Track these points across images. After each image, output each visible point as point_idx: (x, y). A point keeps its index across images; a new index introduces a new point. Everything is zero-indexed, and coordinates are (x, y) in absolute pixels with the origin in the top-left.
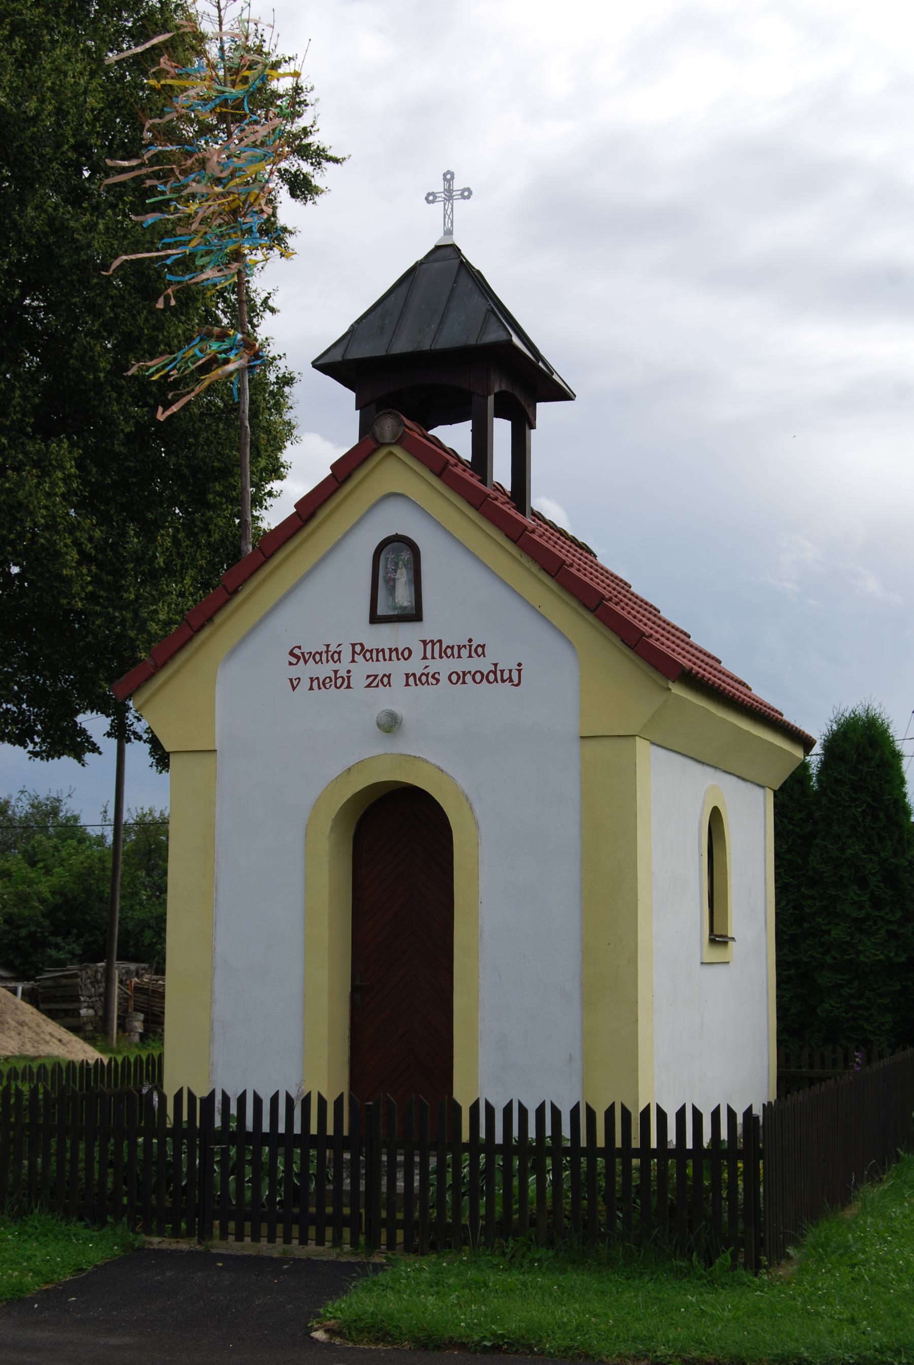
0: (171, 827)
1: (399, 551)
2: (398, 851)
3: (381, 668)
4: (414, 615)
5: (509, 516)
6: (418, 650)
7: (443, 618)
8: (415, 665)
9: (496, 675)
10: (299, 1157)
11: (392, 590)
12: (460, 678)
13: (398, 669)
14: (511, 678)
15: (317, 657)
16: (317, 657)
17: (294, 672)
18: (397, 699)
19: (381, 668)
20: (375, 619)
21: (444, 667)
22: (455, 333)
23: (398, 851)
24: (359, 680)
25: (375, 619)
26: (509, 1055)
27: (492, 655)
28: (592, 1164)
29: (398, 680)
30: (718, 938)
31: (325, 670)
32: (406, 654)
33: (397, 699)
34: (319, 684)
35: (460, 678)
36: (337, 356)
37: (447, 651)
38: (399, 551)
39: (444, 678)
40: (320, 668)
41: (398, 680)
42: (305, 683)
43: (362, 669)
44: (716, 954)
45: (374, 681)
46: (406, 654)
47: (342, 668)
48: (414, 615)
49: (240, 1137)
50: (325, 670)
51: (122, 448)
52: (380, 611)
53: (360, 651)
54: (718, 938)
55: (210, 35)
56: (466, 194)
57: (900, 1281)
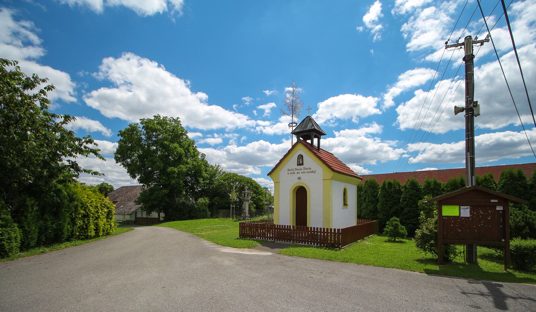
1: (301, 157)
2: (301, 194)
3: (298, 171)
4: (302, 164)
7: (306, 165)
8: (303, 171)
9: (312, 172)
13: (300, 171)
18: (300, 175)
19: (298, 171)
21: (306, 171)
23: (301, 194)
24: (296, 173)
26: (315, 220)
27: (312, 169)
28: (321, 234)
30: (345, 204)
31: (292, 172)
33: (300, 175)
38: (301, 157)
40: (291, 172)
43: (296, 172)
44: (345, 207)
45: (298, 173)
48: (302, 164)
50: (292, 172)
51: (385, 146)
53: (296, 169)
54: (345, 204)
55: (118, 83)
56: (311, 109)
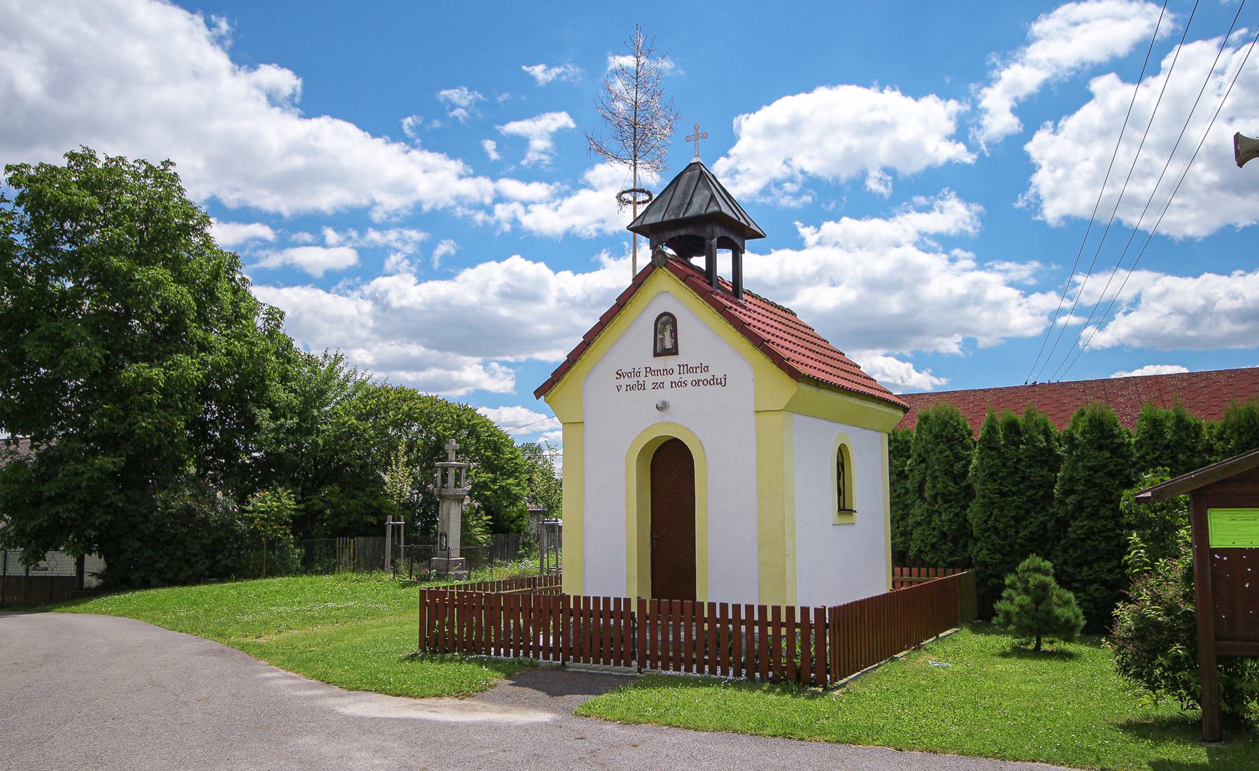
0: (564, 488)
1: (667, 322)
3: (659, 379)
4: (674, 351)
5: (726, 299)
6: (676, 370)
7: (688, 354)
8: (675, 377)
9: (714, 381)
10: (531, 414)
11: (662, 340)
12: (697, 383)
13: (667, 379)
14: (722, 382)
15: (629, 375)
16: (629, 375)
17: (619, 382)
18: (666, 394)
19: (659, 379)
20: (656, 354)
22: (697, 207)
24: (649, 385)
25: (656, 354)
26: (728, 574)
29: (667, 385)
30: (844, 509)
31: (633, 381)
32: (671, 372)
34: (630, 388)
35: (697, 383)
36: (638, 223)
37: (691, 370)
38: (667, 322)
39: (689, 383)
40: (630, 380)
41: (667, 385)
42: (624, 387)
43: (650, 380)
44: (846, 519)
45: (657, 386)
46: (671, 372)
47: (641, 379)
48: (674, 351)
49: (587, 613)
50: (633, 381)
52: (658, 351)
53: (649, 371)
54: (844, 509)
57: (146, 177)
